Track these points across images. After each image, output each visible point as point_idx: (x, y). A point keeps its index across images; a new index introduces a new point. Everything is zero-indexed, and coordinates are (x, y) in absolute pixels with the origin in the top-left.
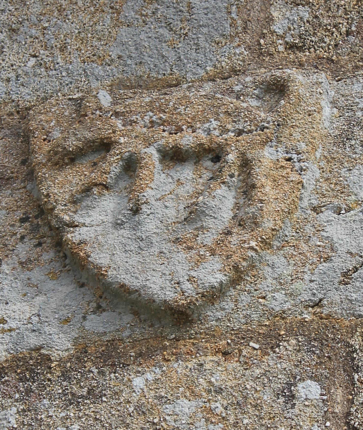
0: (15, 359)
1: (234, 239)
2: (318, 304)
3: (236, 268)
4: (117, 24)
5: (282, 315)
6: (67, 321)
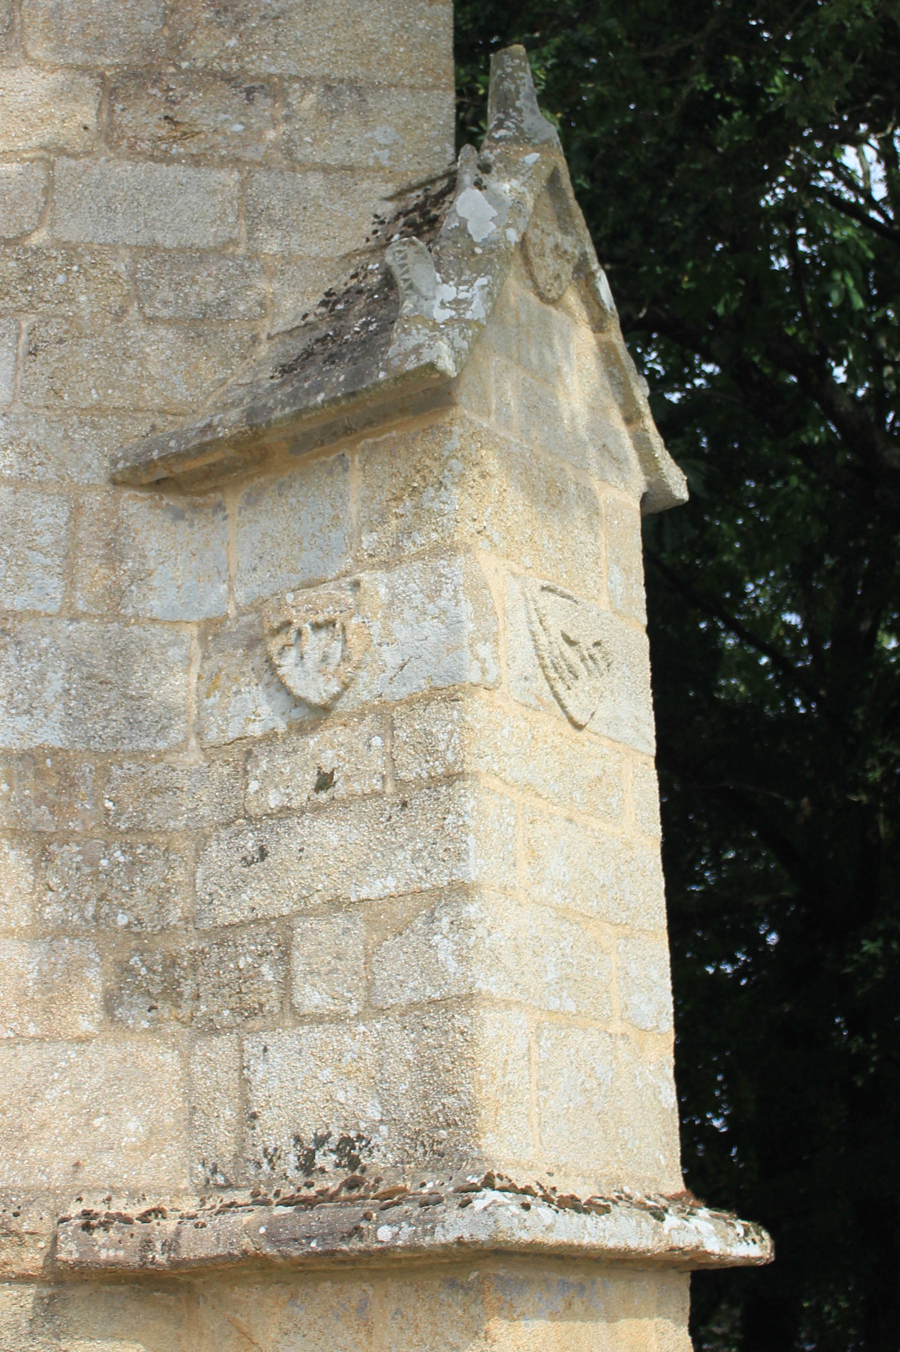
0: (265, 735)
1: (341, 668)
2: (380, 696)
3: (343, 683)
4: (301, 550)
5: (366, 703)
6: (283, 714)
